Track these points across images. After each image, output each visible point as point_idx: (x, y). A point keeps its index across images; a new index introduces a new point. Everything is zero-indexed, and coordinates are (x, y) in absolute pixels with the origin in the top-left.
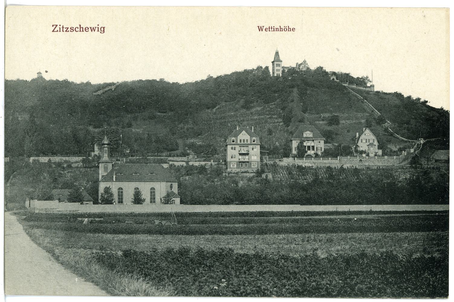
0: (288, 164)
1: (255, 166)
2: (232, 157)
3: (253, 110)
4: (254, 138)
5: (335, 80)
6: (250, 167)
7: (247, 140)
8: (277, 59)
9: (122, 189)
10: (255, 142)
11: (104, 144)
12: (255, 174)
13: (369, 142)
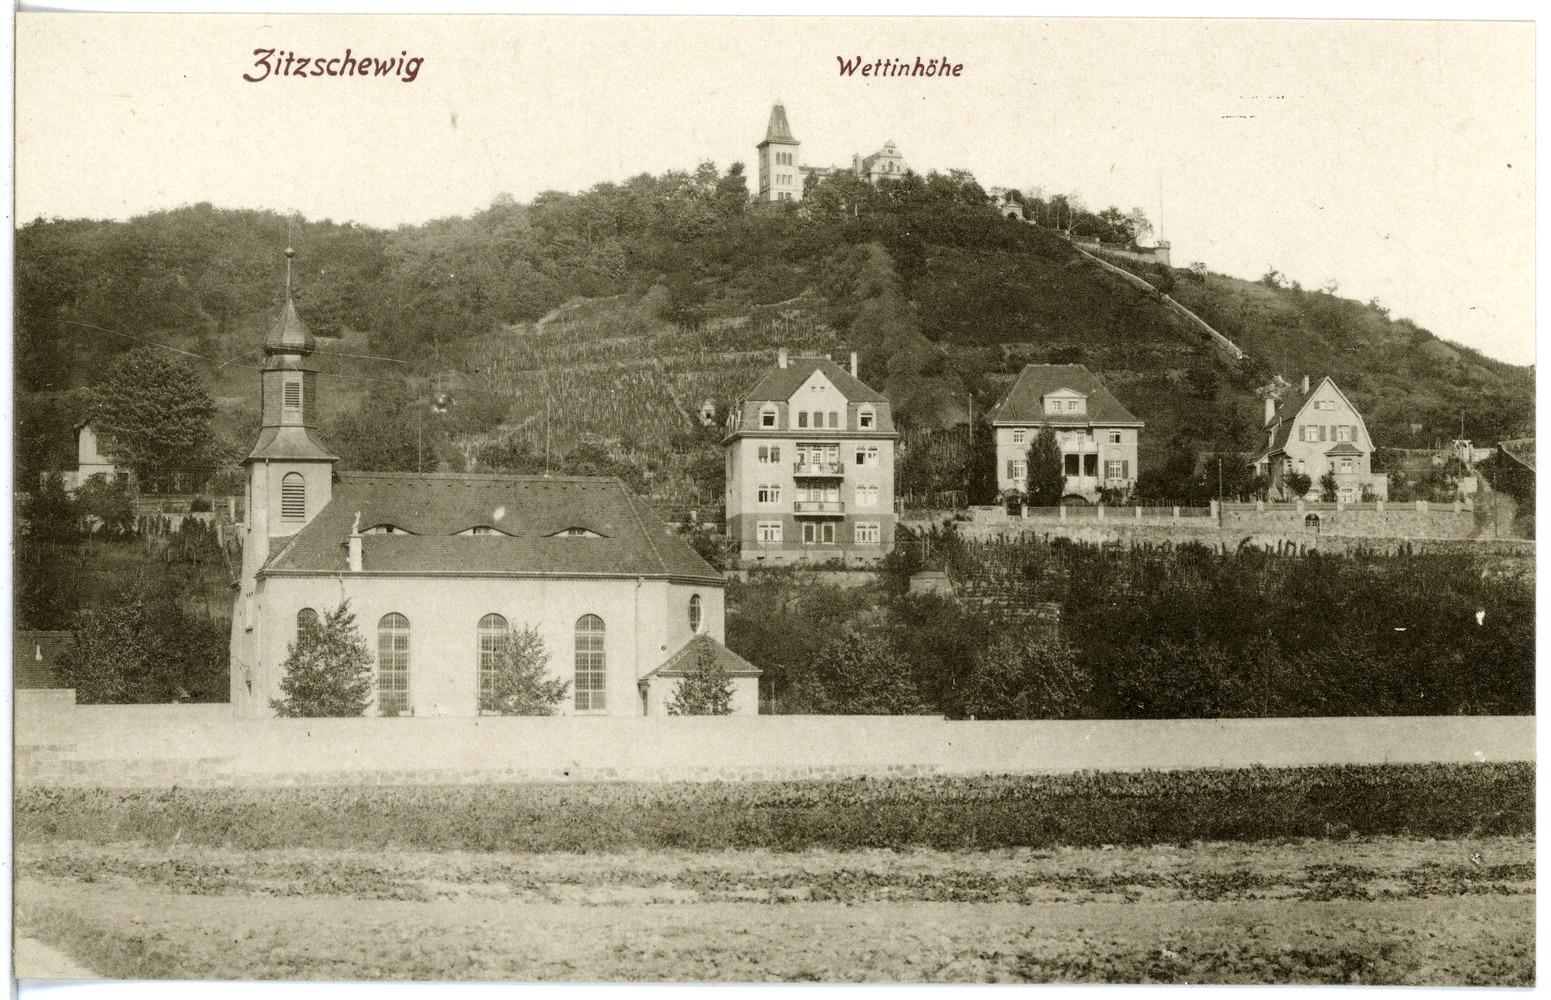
0: (1001, 535)
1: (873, 542)
2: (761, 493)
3: (713, 326)
4: (866, 407)
5: (1020, 217)
6: (848, 542)
7: (834, 415)
8: (777, 137)
9: (402, 621)
10: (872, 427)
11: (283, 350)
12: (872, 575)
13: (1334, 439)
